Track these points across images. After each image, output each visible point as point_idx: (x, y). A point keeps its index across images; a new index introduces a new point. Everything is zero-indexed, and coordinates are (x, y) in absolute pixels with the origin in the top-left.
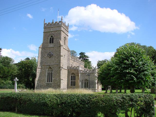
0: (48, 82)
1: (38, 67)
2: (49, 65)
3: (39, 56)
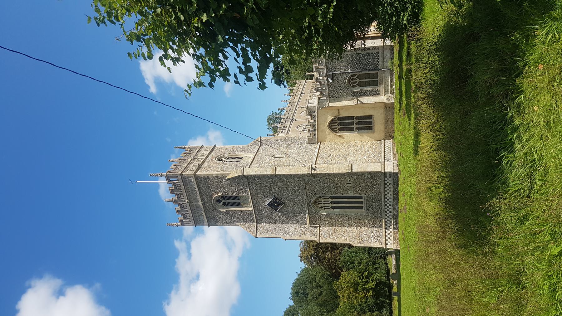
0: (362, 208)
1: (317, 240)
2: (309, 205)
3: (282, 237)
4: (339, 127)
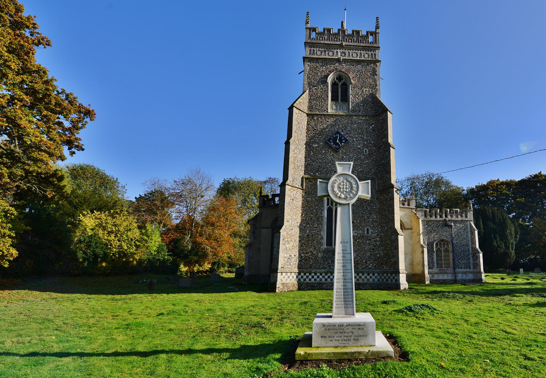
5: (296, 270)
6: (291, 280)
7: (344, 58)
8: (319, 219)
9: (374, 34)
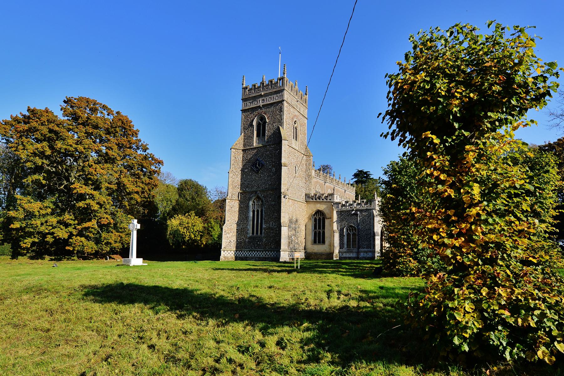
4: (317, 219)
5: (235, 249)
6: (230, 255)
7: (264, 104)
8: (247, 217)
9: (282, 79)
